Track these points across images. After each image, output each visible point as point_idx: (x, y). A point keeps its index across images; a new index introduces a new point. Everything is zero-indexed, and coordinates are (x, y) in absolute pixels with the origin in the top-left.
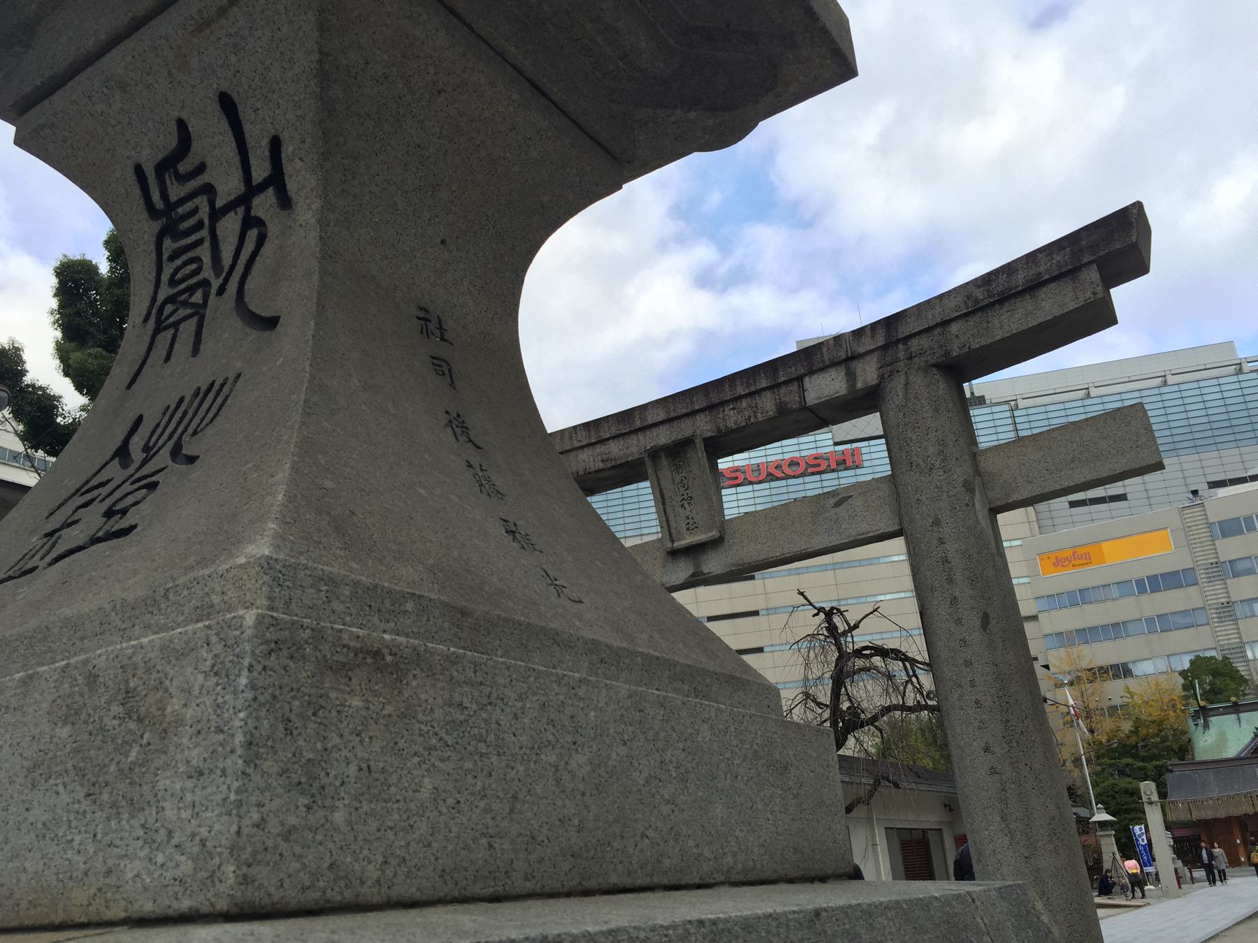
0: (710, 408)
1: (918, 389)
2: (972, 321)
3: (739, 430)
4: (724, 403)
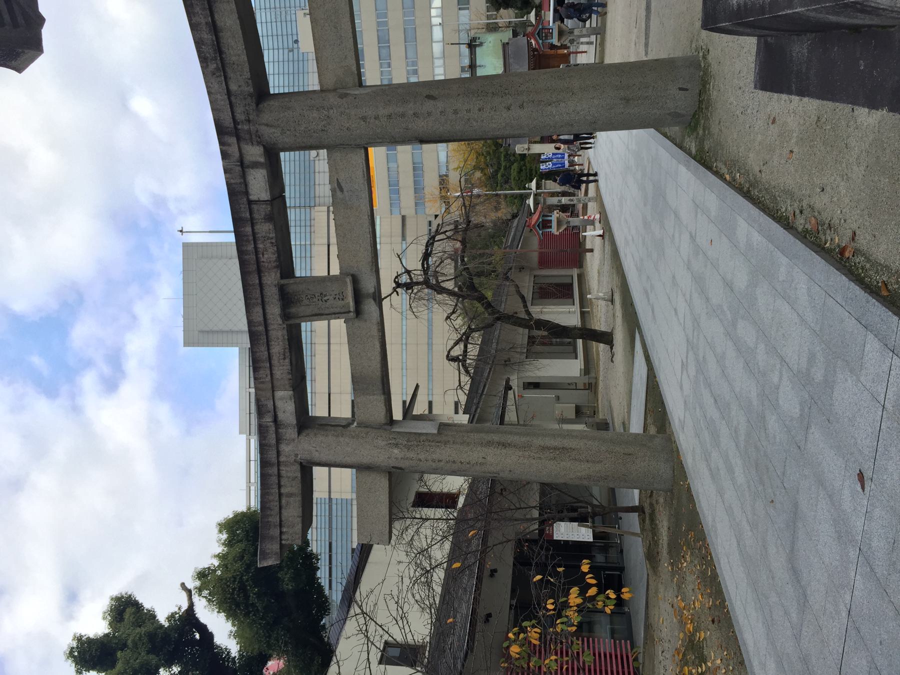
0: (259, 272)
1: (270, 123)
2: (231, 74)
3: (278, 251)
4: (258, 262)
